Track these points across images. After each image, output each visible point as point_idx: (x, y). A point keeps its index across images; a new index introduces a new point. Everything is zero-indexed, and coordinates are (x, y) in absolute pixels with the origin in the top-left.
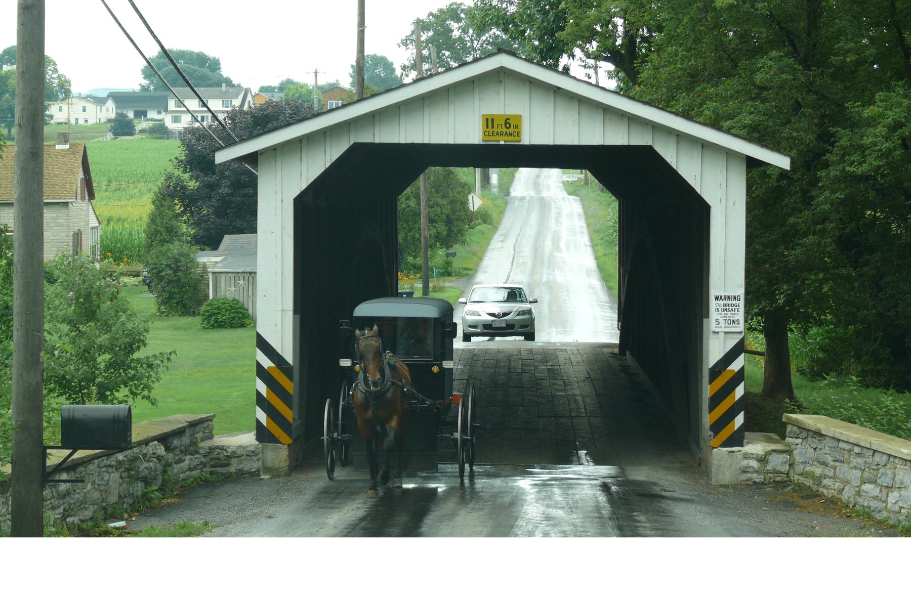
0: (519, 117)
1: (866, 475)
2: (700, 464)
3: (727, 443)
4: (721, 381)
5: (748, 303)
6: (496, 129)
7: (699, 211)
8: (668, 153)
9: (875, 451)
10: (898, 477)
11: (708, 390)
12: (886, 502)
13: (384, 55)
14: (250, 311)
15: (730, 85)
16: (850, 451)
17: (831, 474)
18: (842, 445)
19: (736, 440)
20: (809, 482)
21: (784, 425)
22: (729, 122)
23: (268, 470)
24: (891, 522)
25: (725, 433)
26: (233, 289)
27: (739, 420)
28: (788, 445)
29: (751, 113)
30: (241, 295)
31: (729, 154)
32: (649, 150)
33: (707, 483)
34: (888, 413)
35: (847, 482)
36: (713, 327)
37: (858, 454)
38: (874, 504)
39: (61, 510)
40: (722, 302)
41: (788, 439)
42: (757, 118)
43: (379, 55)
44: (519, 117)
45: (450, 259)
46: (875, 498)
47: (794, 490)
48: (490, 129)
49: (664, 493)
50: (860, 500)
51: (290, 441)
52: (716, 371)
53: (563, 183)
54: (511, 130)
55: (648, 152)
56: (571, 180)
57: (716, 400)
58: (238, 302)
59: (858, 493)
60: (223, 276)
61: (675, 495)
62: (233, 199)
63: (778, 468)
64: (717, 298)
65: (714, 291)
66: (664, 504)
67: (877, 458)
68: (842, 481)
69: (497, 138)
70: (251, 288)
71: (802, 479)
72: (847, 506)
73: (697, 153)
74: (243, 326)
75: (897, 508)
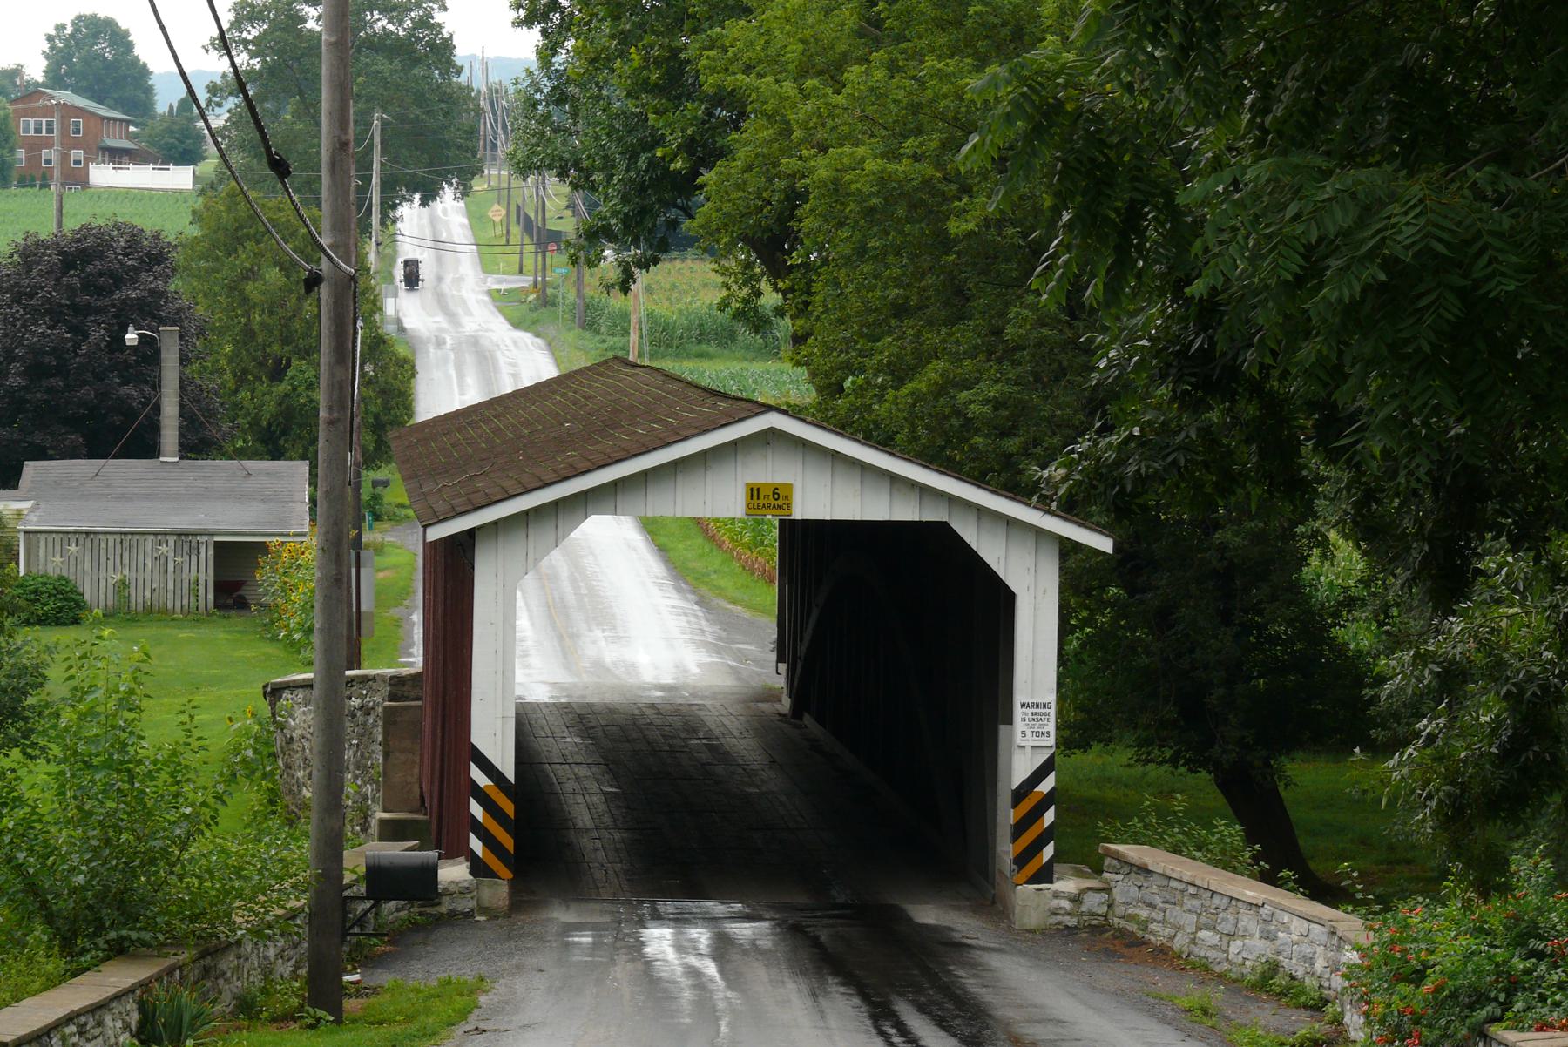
0: (789, 487)
1: (1203, 920)
2: (994, 903)
3: (1033, 880)
4: (1027, 805)
5: (1060, 714)
6: (761, 501)
7: (1001, 601)
8: (968, 532)
9: (1214, 893)
10: (1241, 924)
11: (1007, 816)
12: (1227, 952)
13: (111, 15)
14: (87, 597)
15: (967, 334)
16: (1182, 891)
17: (1160, 918)
18: (1173, 884)
19: (1044, 875)
20: (1132, 927)
21: (1101, 858)
22: (965, 393)
23: (483, 910)
24: (1234, 976)
25: (1032, 867)
26: (58, 559)
27: (1048, 852)
28: (1106, 882)
29: (997, 381)
30: (72, 570)
31: (1039, 533)
32: (944, 527)
33: (1010, 929)
34: (1221, 840)
35: (1179, 928)
36: (1019, 740)
37: (1193, 896)
38: (1212, 954)
39: (293, 962)
40: (1029, 711)
41: (1105, 875)
42: (1006, 389)
43: (102, 15)
44: (789, 487)
45: (379, 489)
46: (1214, 947)
47: (1115, 937)
48: (755, 501)
49: (969, 942)
50: (1196, 950)
51: (511, 876)
52: (1020, 794)
53: (490, 293)
54: (780, 502)
55: (942, 531)
56: (503, 287)
57: (1019, 829)
58: (68, 581)
59: (1194, 941)
60: (42, 537)
61: (981, 943)
62: (28, 396)
63: (1095, 910)
64: (1023, 706)
65: (1020, 697)
66: (976, 955)
67: (1217, 900)
68: (1174, 926)
69: (764, 511)
70: (88, 558)
71: (1123, 923)
72: (1180, 957)
73: (1001, 530)
74: (76, 621)
75: (1240, 960)
